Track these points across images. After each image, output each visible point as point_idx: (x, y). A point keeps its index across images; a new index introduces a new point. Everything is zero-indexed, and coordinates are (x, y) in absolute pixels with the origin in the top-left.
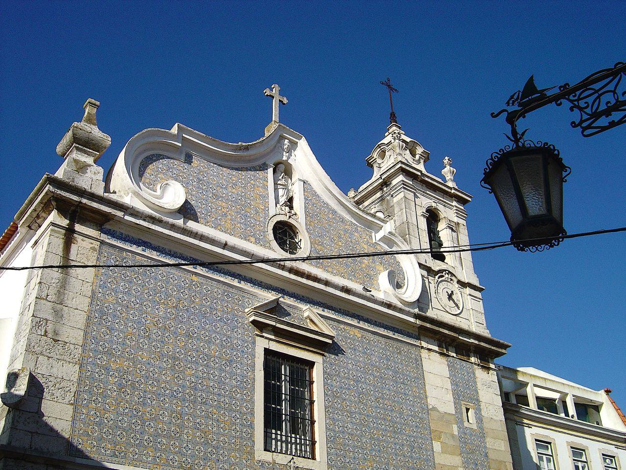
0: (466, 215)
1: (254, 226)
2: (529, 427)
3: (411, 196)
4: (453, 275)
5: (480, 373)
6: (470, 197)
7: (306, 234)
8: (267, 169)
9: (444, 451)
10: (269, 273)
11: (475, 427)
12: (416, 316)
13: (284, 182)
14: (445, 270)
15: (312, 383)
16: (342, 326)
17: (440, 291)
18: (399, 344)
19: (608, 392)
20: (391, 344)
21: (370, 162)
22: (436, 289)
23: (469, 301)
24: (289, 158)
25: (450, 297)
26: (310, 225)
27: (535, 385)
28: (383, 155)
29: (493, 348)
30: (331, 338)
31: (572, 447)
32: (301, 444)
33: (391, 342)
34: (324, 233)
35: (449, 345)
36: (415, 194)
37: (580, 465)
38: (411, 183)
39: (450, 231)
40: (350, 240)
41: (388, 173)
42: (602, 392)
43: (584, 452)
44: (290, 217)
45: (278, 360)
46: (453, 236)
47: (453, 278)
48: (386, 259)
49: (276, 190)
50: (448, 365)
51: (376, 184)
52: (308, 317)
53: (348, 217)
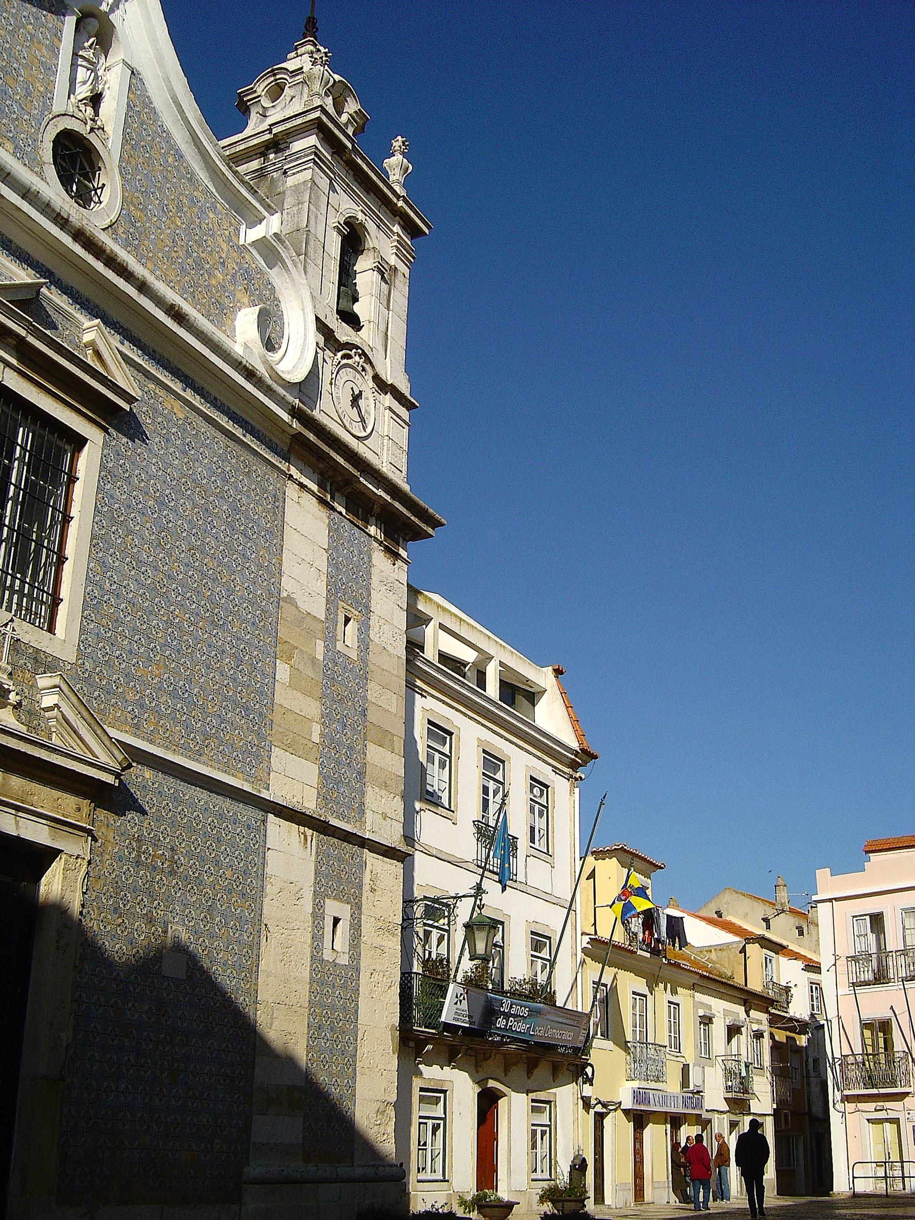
0: (414, 258)
1: (17, 119)
2: (422, 696)
3: (324, 183)
4: (368, 360)
5: (379, 558)
6: (429, 227)
7: (118, 177)
8: (64, 16)
9: (292, 685)
10: (30, 225)
11: (354, 655)
12: (295, 413)
13: (92, 56)
14: (357, 347)
15: (73, 480)
16: (152, 386)
17: (340, 382)
18: (251, 457)
19: (558, 672)
20: (236, 452)
21: (245, 99)
22: (334, 376)
23: (386, 421)
24: (112, 10)
25: (356, 399)
26: (128, 163)
27: (442, 627)
28: (277, 92)
29: (413, 518)
30: (130, 399)
31: (484, 751)
32: (30, 596)
33: (237, 448)
34: (152, 190)
35: (337, 490)
36: (331, 181)
37: (492, 786)
38: (330, 158)
39: (376, 276)
40: (198, 221)
41: (288, 125)
42: (549, 671)
43: (502, 765)
44: (92, 130)
45: (14, 415)
46: (382, 290)
47: (367, 367)
48: (256, 286)
49: (74, 66)
50: (329, 525)
51: (255, 142)
52: (92, 344)
53: (202, 175)
